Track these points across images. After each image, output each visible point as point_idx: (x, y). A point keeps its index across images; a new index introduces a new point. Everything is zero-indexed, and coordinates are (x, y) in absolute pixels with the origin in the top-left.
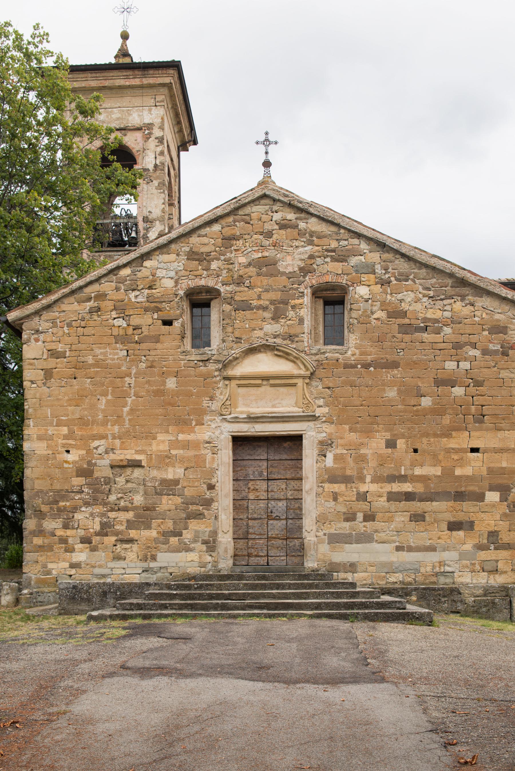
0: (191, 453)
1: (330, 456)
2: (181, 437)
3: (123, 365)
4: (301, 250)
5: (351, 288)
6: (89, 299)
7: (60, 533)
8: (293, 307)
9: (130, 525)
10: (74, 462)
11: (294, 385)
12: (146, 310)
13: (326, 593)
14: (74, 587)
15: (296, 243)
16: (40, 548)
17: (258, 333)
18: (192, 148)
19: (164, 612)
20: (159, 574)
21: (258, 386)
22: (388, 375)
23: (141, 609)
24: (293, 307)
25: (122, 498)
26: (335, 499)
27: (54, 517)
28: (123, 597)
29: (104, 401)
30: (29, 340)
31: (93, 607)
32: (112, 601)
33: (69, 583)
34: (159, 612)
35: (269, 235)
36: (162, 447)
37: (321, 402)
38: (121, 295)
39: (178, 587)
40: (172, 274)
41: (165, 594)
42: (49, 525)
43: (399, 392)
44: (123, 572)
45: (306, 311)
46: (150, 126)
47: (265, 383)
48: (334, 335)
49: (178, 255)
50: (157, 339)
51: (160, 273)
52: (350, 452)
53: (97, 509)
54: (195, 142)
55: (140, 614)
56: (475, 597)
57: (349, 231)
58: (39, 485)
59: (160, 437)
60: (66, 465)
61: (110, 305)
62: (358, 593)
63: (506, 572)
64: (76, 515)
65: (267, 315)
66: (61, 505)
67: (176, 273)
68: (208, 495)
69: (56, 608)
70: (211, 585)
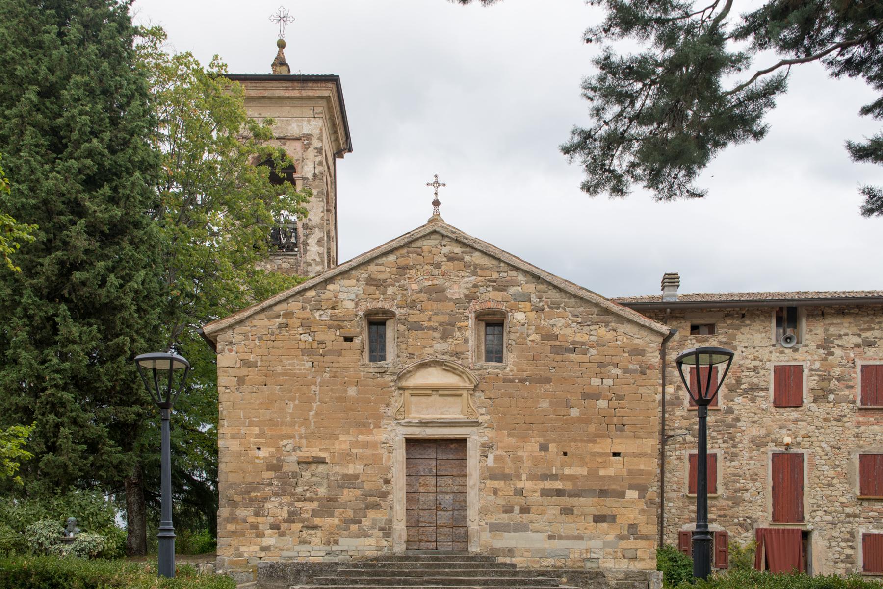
0: (370, 452)
1: (491, 457)
2: (361, 438)
6: (278, 316)
7: (251, 520)
8: (460, 329)
9: (315, 513)
11: (460, 395)
12: (330, 327)
13: (492, 572)
14: (271, 566)
15: (462, 274)
16: (233, 533)
17: (428, 350)
18: (347, 155)
20: (341, 557)
21: (429, 395)
24: (460, 329)
26: (495, 494)
27: (246, 506)
29: (292, 406)
30: (223, 351)
35: (438, 265)
36: (343, 447)
38: (307, 314)
40: (353, 297)
42: (241, 513)
43: (551, 403)
45: (470, 333)
46: (309, 137)
47: (434, 393)
48: (495, 354)
49: (358, 280)
51: (342, 296)
53: (285, 500)
58: (232, 478)
59: (342, 438)
60: (257, 461)
61: (297, 322)
62: (518, 572)
63: (644, 559)
64: (266, 504)
65: (437, 335)
67: (357, 296)
68: (384, 488)
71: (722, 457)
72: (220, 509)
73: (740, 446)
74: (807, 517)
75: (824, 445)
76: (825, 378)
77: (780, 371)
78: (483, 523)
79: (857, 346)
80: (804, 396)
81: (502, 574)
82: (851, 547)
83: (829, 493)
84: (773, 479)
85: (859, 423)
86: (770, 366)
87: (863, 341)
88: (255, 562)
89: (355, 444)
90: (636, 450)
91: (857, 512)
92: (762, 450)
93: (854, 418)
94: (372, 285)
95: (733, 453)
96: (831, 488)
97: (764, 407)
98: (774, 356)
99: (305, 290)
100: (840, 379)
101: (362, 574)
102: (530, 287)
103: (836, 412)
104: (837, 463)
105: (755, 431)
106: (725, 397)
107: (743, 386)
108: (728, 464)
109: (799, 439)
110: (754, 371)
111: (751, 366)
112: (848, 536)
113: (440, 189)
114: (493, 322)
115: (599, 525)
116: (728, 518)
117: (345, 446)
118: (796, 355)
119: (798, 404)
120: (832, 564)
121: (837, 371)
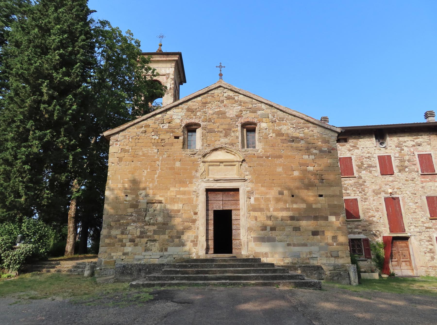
0: (186, 197)
1: (252, 199)
2: (182, 189)
3: (155, 156)
4: (236, 108)
5: (258, 124)
6: (142, 127)
7: (119, 236)
8: (234, 131)
9: (155, 232)
10: (129, 201)
11: (234, 165)
12: (167, 132)
13: (260, 270)
14: (124, 266)
15: (235, 105)
16: (109, 245)
17: (217, 142)
18: (184, 84)
19: (172, 282)
20: (169, 259)
21: (220, 165)
22: (278, 161)
23: (160, 280)
24: (234, 131)
25: (151, 219)
26: (256, 219)
27: (117, 228)
28: (150, 273)
29: (146, 172)
30: (112, 145)
31: (133, 278)
32: (143, 274)
33: (121, 264)
34: (169, 282)
35: (222, 102)
36: (172, 194)
37: (247, 173)
38: (156, 126)
39: (180, 267)
40: (180, 117)
41: (173, 271)
42: (114, 232)
43: (283, 169)
44: (150, 257)
46: (168, 74)
47: (221, 164)
49: (183, 109)
50: (172, 144)
51: (174, 117)
52: (262, 196)
53: (139, 225)
54: (185, 82)
55: (159, 284)
56: (330, 271)
57: (257, 100)
59: (172, 189)
60: (125, 202)
61: (151, 130)
62: (277, 270)
63: (343, 257)
64: (128, 227)
65: (222, 135)
66: (120, 223)
67: (182, 117)
68: (194, 217)
69: (113, 278)
70: (197, 265)
71: (360, 200)
72: (103, 230)
73: (368, 194)
74: (406, 228)
75: (408, 193)
76: (402, 161)
77: (381, 158)
78: (249, 237)
79: (414, 146)
80: (394, 169)
81: (267, 271)
82: (432, 245)
83: (415, 217)
84: (387, 210)
85: (422, 181)
86: (376, 156)
87: (416, 143)
88: (119, 262)
89: (179, 192)
90: (331, 193)
91: (431, 226)
92: (379, 196)
93: (419, 179)
94: (189, 111)
95: (365, 198)
96: (415, 214)
97: (376, 175)
98: (377, 151)
99: (156, 114)
100: (409, 161)
101: (177, 272)
102: (269, 111)
103: (410, 177)
104: (416, 201)
105: (374, 187)
106: (357, 171)
107: (365, 166)
108: (363, 203)
109: (395, 190)
110: (369, 158)
111: (367, 156)
112: (429, 239)
113: (222, 69)
114: (249, 128)
115: (315, 237)
116: (367, 231)
117: (173, 194)
118: (387, 151)
119: (392, 174)
120: (424, 254)
121: (407, 158)
